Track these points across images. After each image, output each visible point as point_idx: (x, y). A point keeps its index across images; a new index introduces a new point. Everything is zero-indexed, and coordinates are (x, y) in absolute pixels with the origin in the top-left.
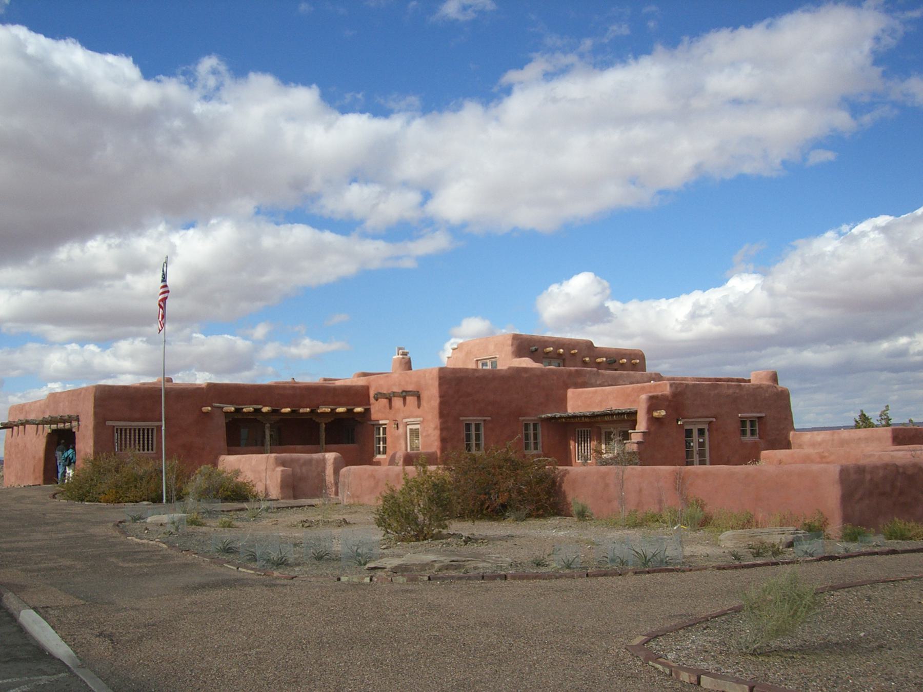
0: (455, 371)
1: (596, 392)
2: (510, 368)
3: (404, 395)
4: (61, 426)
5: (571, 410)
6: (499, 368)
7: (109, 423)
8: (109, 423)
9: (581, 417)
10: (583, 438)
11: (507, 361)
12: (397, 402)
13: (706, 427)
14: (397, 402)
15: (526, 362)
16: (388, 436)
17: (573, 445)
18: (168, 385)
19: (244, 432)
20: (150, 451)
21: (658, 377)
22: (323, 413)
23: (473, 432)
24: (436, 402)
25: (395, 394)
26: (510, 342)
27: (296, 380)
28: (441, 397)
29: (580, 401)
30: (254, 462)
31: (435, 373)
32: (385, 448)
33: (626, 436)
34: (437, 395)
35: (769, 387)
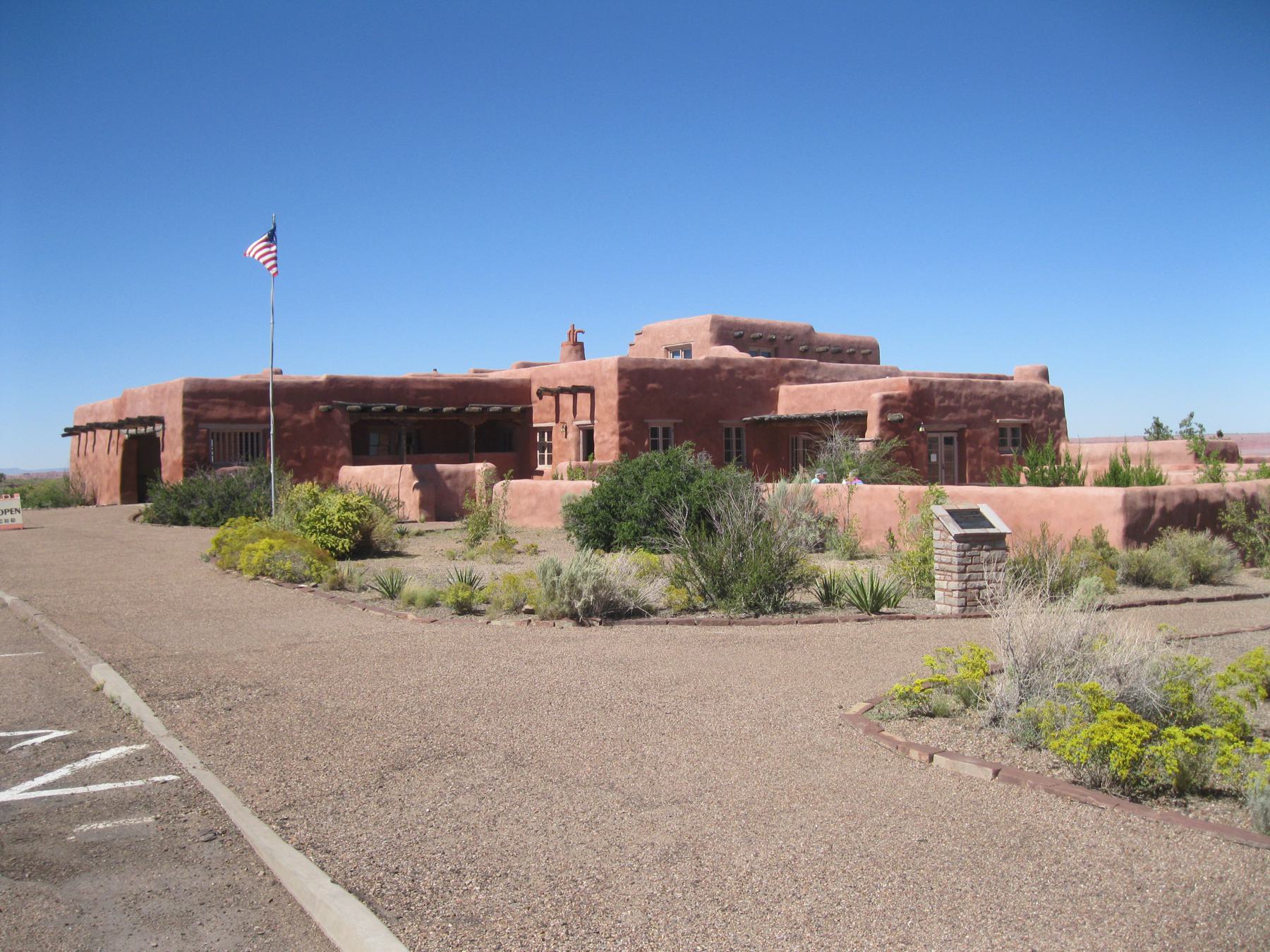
3: (575, 391)
4: (142, 430)
11: (707, 351)
12: (566, 400)
13: (955, 435)
16: (554, 442)
18: (278, 378)
19: (374, 439)
21: (894, 373)
22: (473, 414)
26: (708, 326)
27: (440, 372)
28: (620, 394)
29: (792, 400)
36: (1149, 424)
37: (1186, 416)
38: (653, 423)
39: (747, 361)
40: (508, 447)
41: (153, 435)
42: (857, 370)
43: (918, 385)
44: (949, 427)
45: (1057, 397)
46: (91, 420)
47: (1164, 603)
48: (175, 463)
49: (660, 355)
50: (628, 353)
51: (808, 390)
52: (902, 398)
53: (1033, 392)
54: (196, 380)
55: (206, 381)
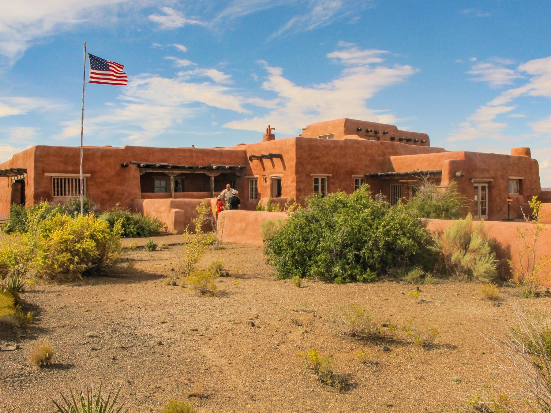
1: (406, 159)
3: (271, 157)
8: (47, 174)
11: (340, 136)
12: (267, 163)
13: (486, 185)
15: (354, 137)
19: (157, 183)
20: (393, 185)
23: (319, 185)
24: (293, 163)
26: (343, 124)
28: (297, 158)
30: (156, 205)
31: (293, 141)
34: (295, 157)
49: (317, 138)
51: (401, 159)
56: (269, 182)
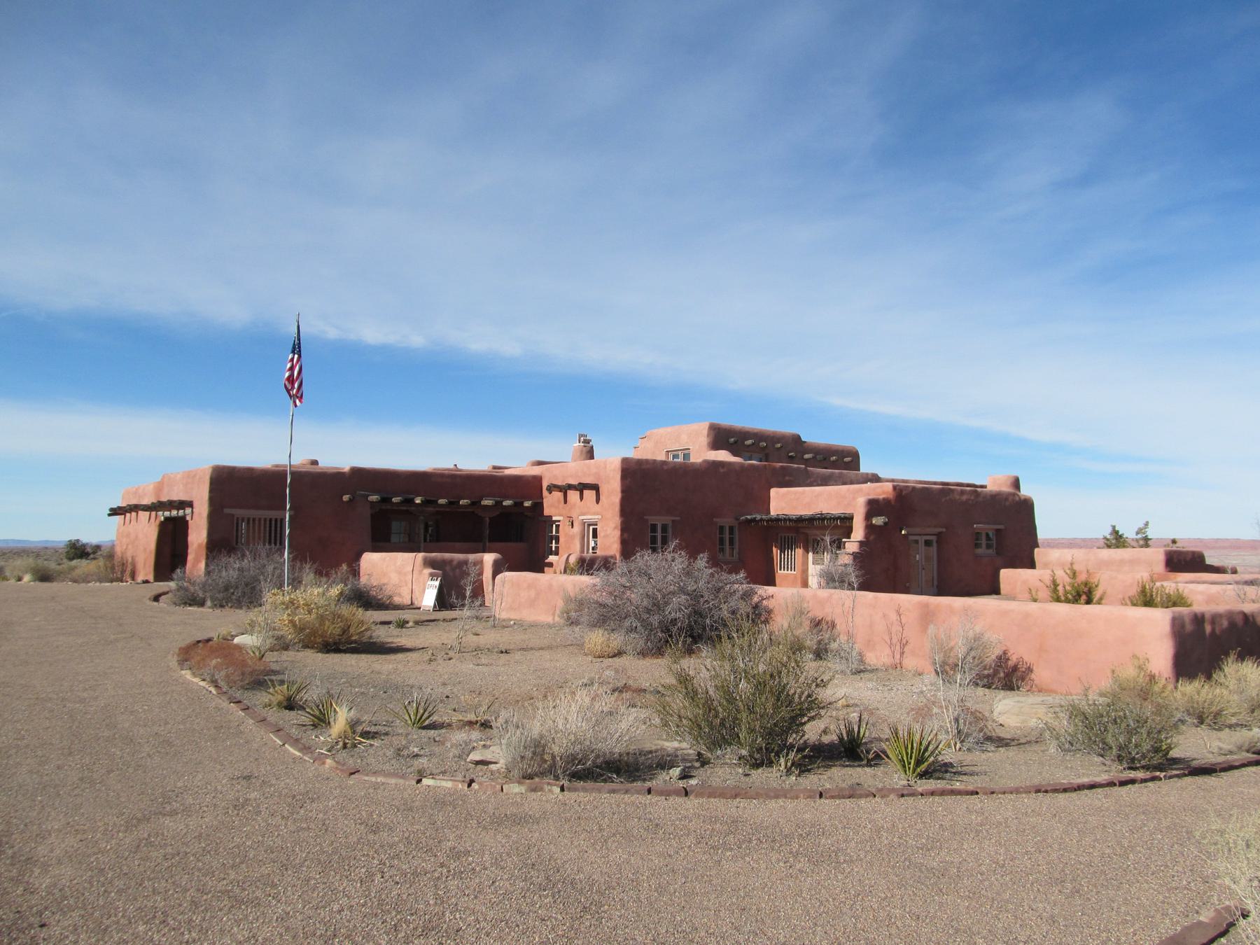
0: (640, 462)
1: (803, 493)
2: (705, 461)
3: (582, 488)
4: (174, 513)
5: (773, 513)
6: (692, 460)
7: (227, 511)
8: (227, 511)
9: (785, 520)
10: (787, 545)
11: (701, 453)
12: (573, 496)
13: (934, 538)
14: (573, 496)
15: (723, 456)
16: (561, 535)
17: (776, 551)
19: (395, 526)
21: (875, 479)
23: (727, 536)
24: (616, 498)
25: (570, 487)
26: (705, 432)
28: (623, 491)
29: (786, 502)
32: (557, 548)
33: (840, 546)
35: (1010, 494)
36: (1107, 532)
37: (1142, 526)
38: (653, 519)
39: (742, 466)
40: (519, 538)
41: (184, 518)
42: (841, 476)
43: (901, 491)
44: (929, 530)
45: (1027, 507)
46: (134, 502)
47: (1133, 781)
48: (200, 546)
50: (631, 454)
52: (887, 502)
53: (1006, 499)
54: (224, 467)
55: (234, 468)
56: (577, 529)
